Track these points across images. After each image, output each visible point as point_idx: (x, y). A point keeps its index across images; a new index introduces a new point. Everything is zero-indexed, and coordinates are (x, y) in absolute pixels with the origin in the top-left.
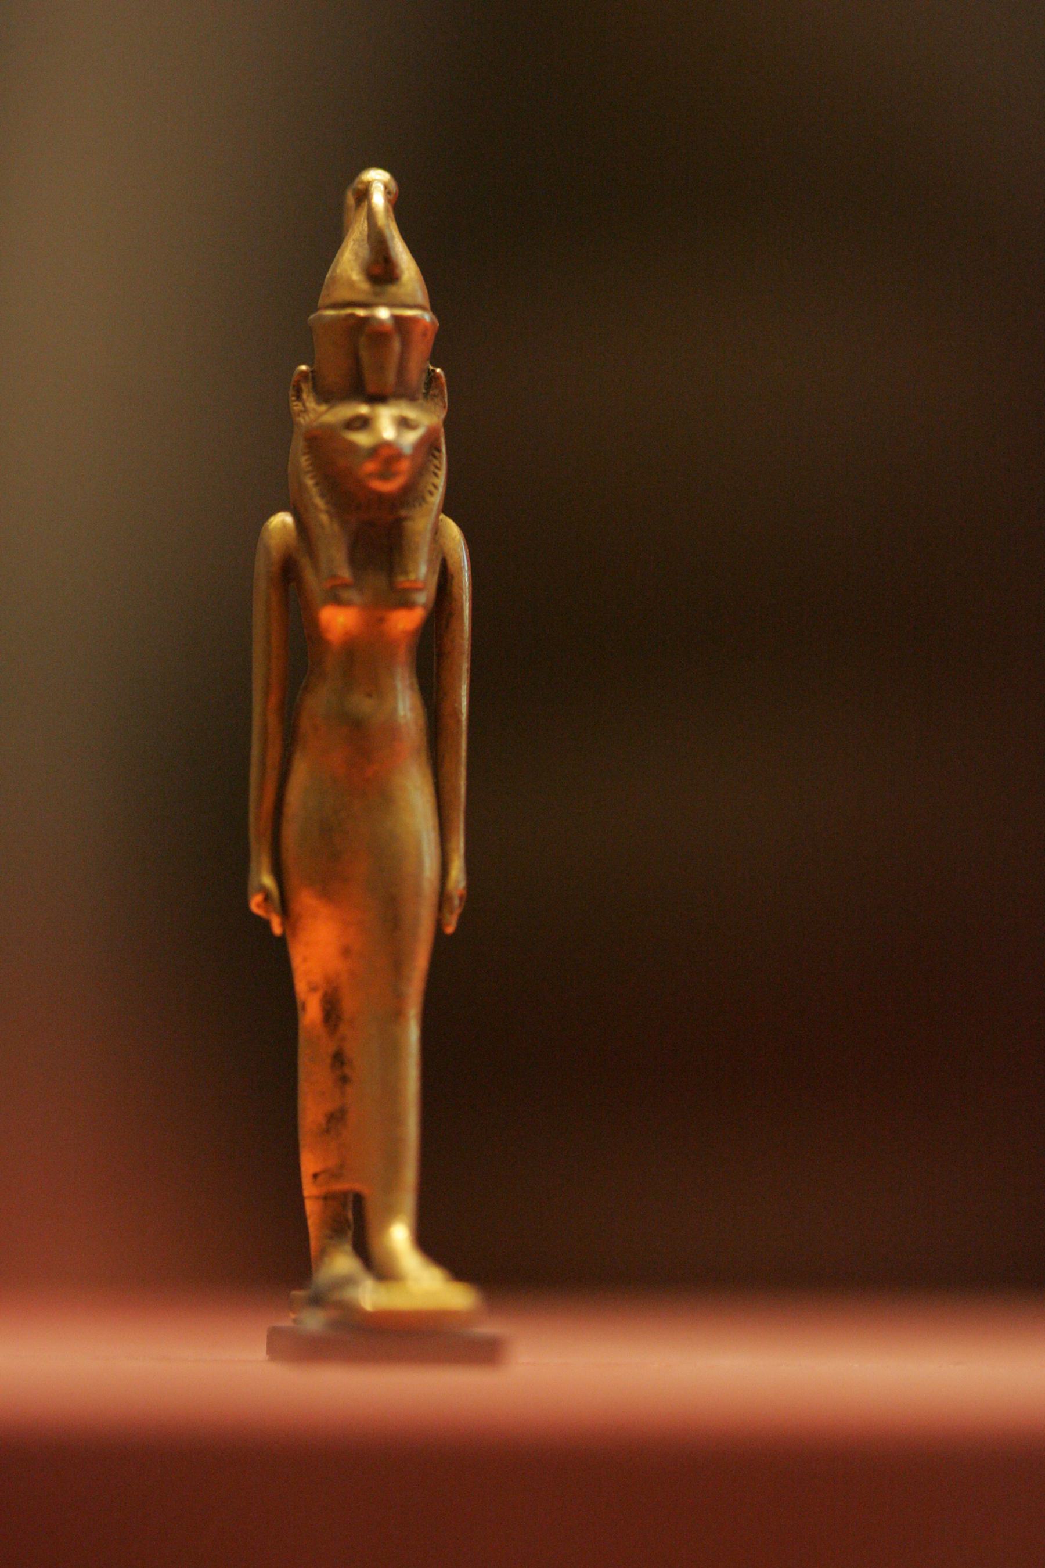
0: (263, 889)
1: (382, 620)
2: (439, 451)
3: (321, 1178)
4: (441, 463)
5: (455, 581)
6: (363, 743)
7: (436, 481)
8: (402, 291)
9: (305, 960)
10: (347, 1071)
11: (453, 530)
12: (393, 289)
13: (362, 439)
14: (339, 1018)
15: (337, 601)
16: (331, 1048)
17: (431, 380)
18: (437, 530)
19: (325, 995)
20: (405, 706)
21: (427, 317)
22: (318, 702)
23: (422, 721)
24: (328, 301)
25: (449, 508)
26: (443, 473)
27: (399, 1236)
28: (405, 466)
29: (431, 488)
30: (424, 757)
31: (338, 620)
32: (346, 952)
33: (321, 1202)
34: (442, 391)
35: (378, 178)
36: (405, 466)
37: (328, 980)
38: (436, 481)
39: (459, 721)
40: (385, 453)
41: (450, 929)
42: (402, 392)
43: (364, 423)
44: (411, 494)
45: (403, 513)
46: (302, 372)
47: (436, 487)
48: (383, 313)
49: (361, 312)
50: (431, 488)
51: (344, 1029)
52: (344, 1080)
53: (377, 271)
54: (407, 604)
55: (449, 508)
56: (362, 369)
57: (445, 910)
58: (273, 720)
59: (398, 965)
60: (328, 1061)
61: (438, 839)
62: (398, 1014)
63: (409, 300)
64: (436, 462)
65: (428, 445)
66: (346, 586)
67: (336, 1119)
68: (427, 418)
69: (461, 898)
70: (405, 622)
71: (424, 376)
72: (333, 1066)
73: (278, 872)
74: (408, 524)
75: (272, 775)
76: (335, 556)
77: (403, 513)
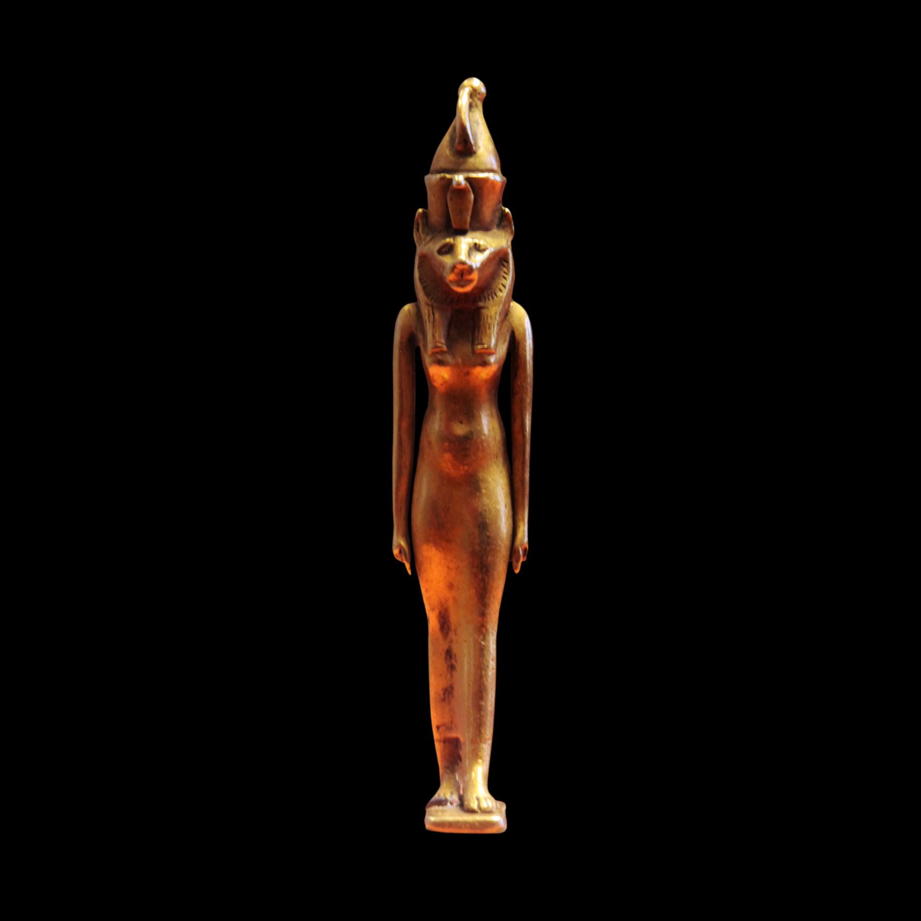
0: (400, 546)
1: (468, 373)
2: (507, 262)
3: (441, 729)
4: (508, 270)
5: (521, 345)
6: (465, 448)
7: (504, 281)
8: (477, 160)
9: (427, 590)
10: (454, 662)
11: (519, 313)
12: (471, 160)
13: (447, 260)
14: (449, 628)
15: (440, 363)
16: (445, 647)
18: (506, 314)
19: (440, 613)
20: (488, 424)
22: (435, 425)
25: (518, 295)
27: (479, 772)
28: (475, 276)
29: (502, 287)
30: (500, 460)
31: (439, 375)
32: (451, 586)
33: (442, 744)
34: (510, 223)
35: (472, 87)
36: (475, 276)
37: (441, 604)
38: (504, 281)
39: (524, 436)
40: (460, 267)
41: (517, 571)
42: (479, 225)
43: (449, 249)
44: (485, 290)
45: (481, 304)
46: (420, 214)
47: (504, 286)
48: (460, 178)
49: (448, 176)
50: (502, 287)
51: (452, 635)
52: (452, 668)
53: (460, 148)
54: (485, 364)
55: (518, 295)
58: (405, 438)
60: (444, 654)
61: (511, 513)
62: (481, 629)
63: (482, 167)
64: (505, 270)
65: (499, 259)
66: (443, 352)
67: (448, 692)
68: (497, 241)
69: (525, 550)
71: (498, 214)
72: (446, 659)
74: (484, 311)
77: (481, 304)
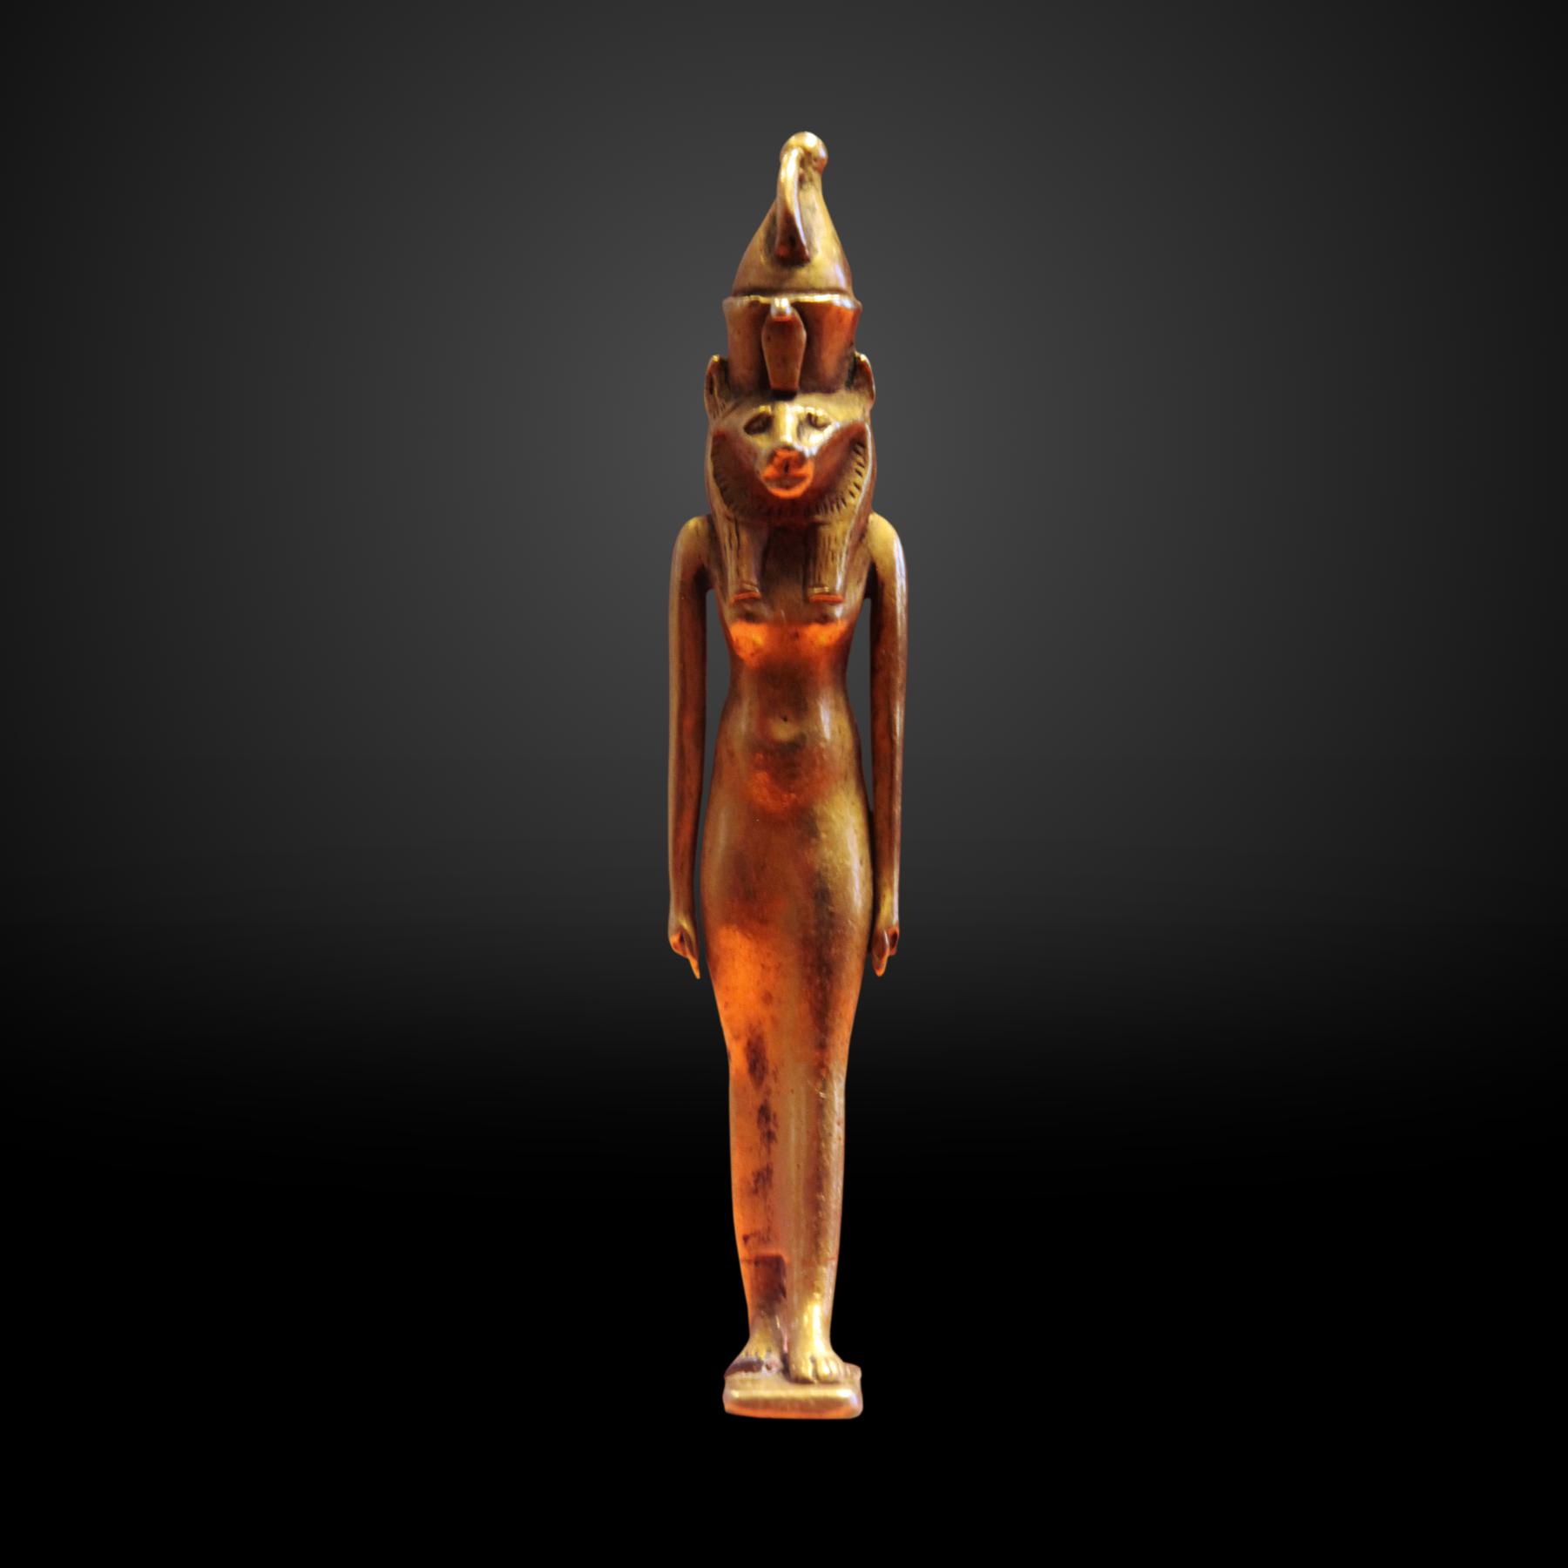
0: (681, 930)
1: (797, 636)
2: (864, 446)
3: (750, 1241)
4: (865, 460)
5: (887, 588)
7: (858, 479)
8: (812, 273)
9: (726, 1005)
10: (772, 1127)
12: (802, 273)
13: (762, 443)
14: (764, 1069)
15: (750, 618)
16: (758, 1101)
17: (858, 367)
18: (862, 534)
19: (749, 1044)
20: (830, 723)
21: (845, 302)
23: (849, 744)
24: (736, 285)
25: (880, 502)
26: (868, 473)
28: (809, 470)
29: (854, 489)
32: (767, 998)
33: (752, 1266)
36: (809, 470)
37: (751, 1029)
38: (858, 479)
39: (892, 742)
40: (783, 454)
41: (880, 973)
42: (815, 383)
43: (765, 425)
44: (826, 493)
45: (819, 518)
47: (858, 487)
48: (782, 304)
49: (763, 300)
50: (854, 489)
51: (769, 1081)
52: (769, 1137)
53: (783, 252)
54: (826, 619)
55: (880, 502)
56: (781, 360)
57: (875, 953)
59: (821, 1013)
60: (755, 1114)
61: (870, 874)
62: (819, 1071)
63: (820, 284)
64: (860, 459)
66: (754, 600)
67: (763, 1179)
70: (742, 723)
71: (847, 365)
72: (759, 1121)
73: (695, 911)
74: (825, 530)
75: (690, 804)
76: (740, 572)
77: (819, 518)
